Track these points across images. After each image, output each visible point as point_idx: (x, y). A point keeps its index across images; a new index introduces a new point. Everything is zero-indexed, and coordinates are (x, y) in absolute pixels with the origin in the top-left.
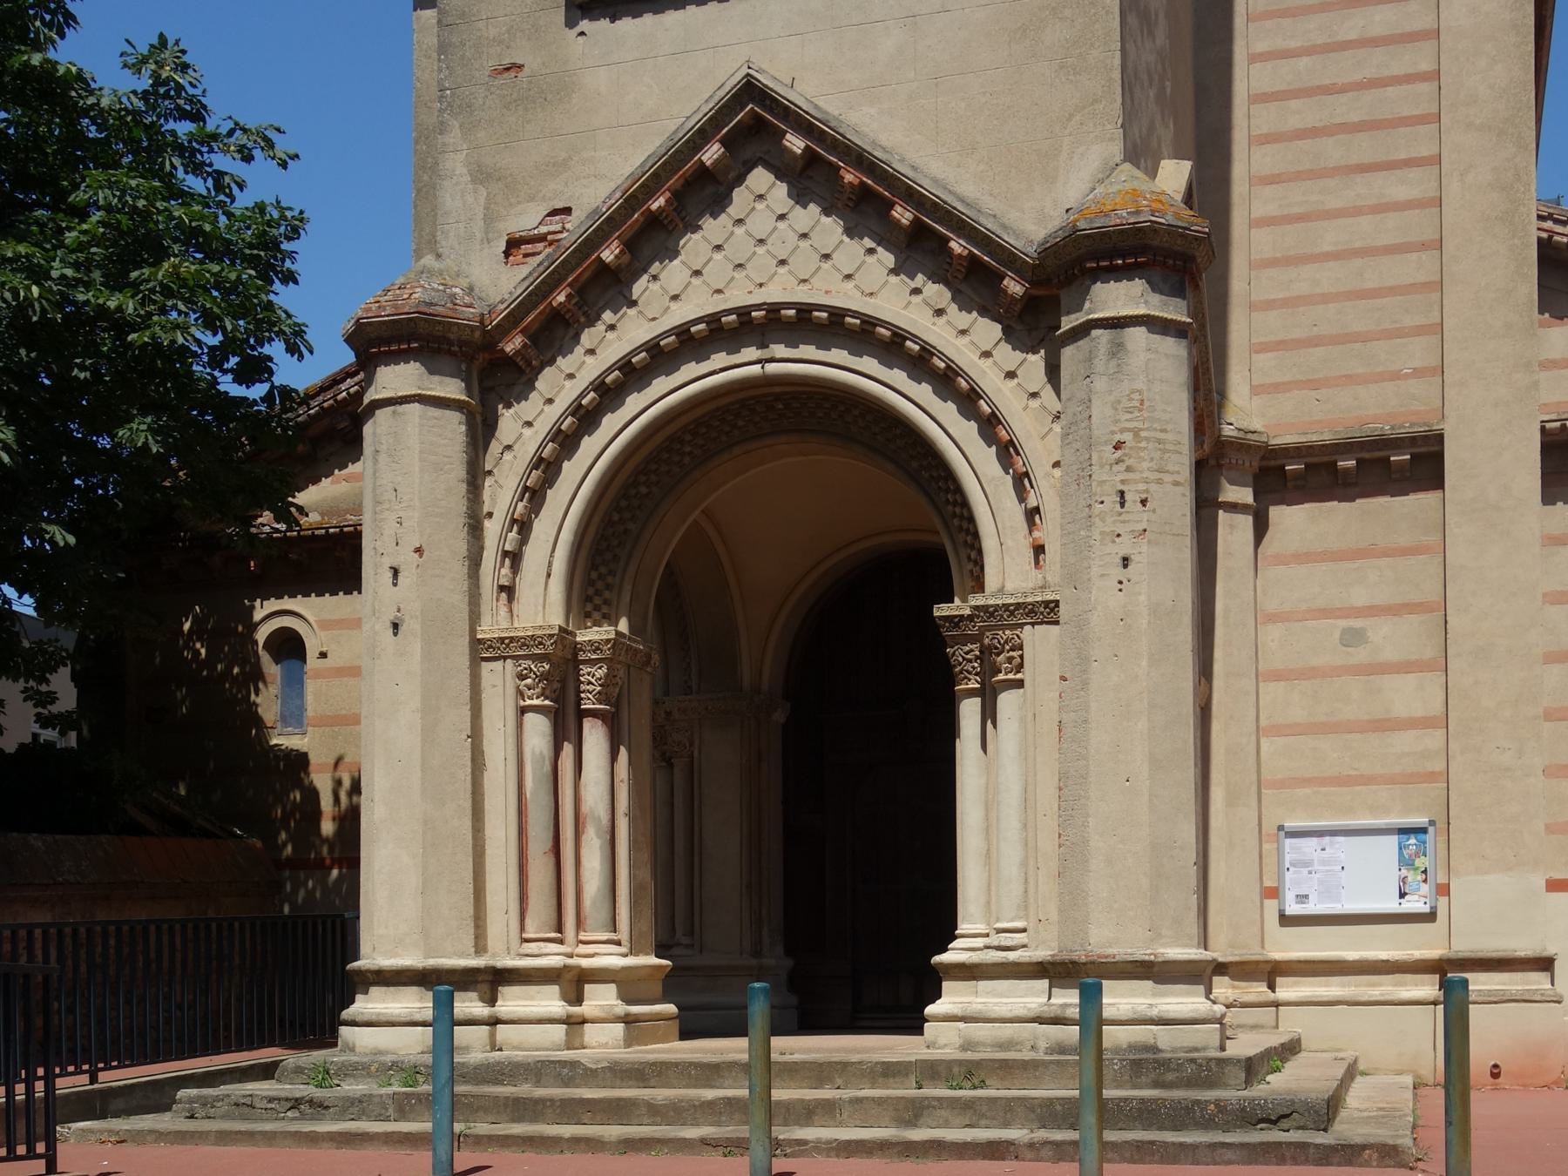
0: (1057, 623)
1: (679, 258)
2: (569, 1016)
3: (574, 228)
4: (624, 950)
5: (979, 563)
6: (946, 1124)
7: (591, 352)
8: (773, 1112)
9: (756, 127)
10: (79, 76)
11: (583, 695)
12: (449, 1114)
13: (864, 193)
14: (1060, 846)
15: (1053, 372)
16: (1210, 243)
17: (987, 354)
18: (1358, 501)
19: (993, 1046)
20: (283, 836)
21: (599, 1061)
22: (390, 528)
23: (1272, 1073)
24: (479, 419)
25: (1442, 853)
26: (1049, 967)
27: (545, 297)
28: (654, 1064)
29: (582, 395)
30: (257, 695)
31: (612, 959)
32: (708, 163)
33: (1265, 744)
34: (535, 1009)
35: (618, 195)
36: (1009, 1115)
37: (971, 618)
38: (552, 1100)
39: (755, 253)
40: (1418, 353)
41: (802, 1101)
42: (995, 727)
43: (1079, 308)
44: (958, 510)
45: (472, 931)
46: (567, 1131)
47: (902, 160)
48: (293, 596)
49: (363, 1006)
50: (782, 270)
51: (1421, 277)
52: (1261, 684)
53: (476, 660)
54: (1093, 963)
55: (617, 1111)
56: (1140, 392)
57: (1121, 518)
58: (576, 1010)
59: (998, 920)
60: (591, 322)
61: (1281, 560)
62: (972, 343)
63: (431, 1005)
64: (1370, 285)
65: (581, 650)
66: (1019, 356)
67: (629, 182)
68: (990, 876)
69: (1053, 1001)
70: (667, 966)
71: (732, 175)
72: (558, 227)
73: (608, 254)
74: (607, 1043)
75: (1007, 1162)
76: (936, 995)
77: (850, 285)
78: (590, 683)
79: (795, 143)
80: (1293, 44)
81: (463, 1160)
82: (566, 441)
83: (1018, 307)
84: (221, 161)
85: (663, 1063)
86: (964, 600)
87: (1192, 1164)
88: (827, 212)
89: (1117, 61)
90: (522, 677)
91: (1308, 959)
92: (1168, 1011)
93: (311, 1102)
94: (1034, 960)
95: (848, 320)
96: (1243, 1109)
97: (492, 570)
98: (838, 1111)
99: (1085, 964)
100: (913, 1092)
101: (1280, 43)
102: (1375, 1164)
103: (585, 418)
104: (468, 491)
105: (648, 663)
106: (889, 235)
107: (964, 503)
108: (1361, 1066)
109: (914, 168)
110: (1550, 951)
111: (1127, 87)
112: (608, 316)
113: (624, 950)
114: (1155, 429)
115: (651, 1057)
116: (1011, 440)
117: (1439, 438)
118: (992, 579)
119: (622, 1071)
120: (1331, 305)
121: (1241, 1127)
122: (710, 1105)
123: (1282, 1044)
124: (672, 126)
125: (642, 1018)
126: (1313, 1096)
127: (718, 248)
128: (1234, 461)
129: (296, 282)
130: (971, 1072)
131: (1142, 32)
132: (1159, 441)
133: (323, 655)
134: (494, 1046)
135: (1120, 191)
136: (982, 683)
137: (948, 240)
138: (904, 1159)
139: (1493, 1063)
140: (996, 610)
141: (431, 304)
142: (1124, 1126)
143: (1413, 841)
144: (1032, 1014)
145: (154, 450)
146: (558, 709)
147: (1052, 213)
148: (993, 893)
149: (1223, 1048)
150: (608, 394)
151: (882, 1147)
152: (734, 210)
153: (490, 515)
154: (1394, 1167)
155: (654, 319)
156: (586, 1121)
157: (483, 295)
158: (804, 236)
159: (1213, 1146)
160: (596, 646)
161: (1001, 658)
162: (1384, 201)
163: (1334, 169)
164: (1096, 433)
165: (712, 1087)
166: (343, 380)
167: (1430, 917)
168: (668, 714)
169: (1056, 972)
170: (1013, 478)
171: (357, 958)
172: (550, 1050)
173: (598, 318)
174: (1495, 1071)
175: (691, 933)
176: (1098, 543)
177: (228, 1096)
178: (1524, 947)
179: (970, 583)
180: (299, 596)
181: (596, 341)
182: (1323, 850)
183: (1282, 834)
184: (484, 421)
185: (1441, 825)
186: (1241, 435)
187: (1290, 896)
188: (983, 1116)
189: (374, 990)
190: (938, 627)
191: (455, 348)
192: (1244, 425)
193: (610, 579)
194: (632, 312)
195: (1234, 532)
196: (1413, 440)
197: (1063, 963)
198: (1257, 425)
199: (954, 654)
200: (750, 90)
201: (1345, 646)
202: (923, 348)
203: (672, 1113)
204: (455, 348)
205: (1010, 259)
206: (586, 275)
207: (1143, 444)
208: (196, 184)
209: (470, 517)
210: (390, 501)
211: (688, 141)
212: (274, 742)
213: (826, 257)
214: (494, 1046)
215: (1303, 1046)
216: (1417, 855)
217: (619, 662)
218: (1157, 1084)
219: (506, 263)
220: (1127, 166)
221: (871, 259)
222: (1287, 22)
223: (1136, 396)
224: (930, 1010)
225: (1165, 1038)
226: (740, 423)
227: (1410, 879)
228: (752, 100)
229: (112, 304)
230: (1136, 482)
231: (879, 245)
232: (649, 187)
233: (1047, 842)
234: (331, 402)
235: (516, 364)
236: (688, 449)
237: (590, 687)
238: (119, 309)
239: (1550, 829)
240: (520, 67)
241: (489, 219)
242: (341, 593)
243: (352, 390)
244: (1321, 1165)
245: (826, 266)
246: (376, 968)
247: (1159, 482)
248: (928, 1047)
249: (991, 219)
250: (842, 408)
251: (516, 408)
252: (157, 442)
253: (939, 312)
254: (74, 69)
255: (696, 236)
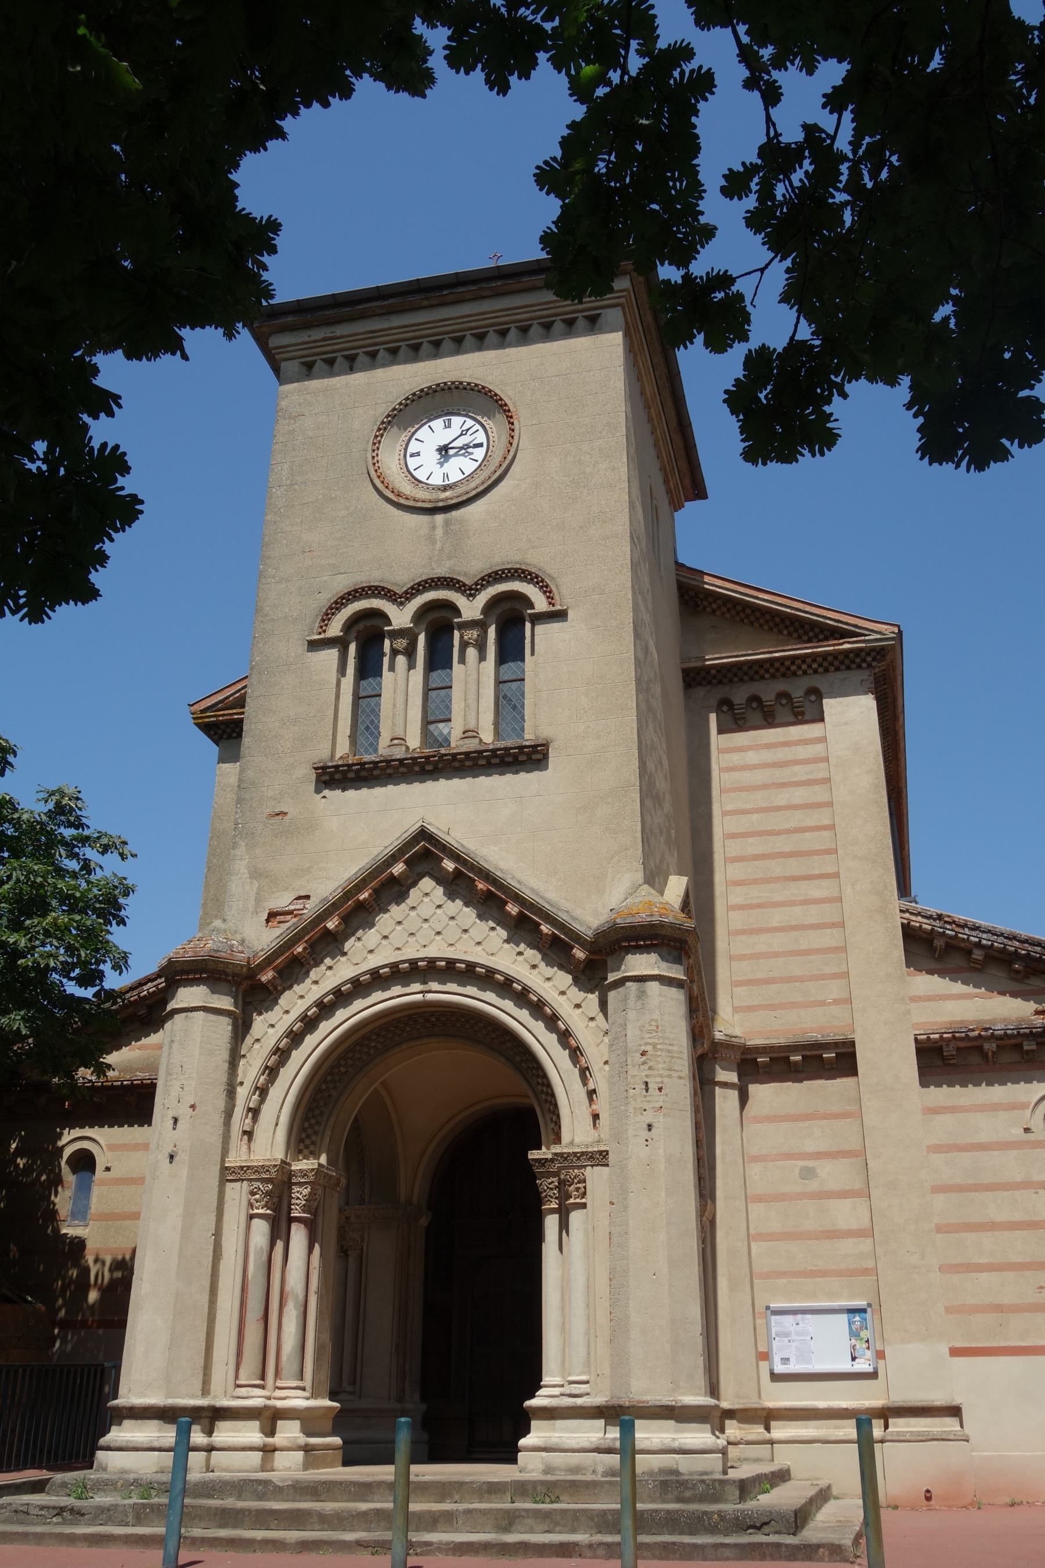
0: (607, 1165)
1: (375, 928)
2: (265, 1446)
3: (311, 908)
4: (307, 1394)
5: (558, 1123)
6: (532, 1531)
7: (316, 982)
8: (409, 1521)
9: (426, 855)
10: (10, 801)
11: (292, 1207)
12: (179, 1517)
13: (489, 896)
14: (611, 1321)
15: (603, 1005)
16: (697, 933)
17: (563, 993)
18: (805, 1082)
19: (565, 1471)
20: (60, 1302)
21: (285, 1480)
22: (175, 1091)
23: (763, 1493)
24: (240, 1022)
25: (878, 1327)
26: (604, 1410)
27: (289, 949)
28: (325, 1483)
29: (308, 1009)
30: (56, 1196)
31: (298, 1401)
32: (396, 874)
33: (754, 1246)
34: (241, 1440)
35: (340, 890)
36: (575, 1523)
37: (552, 1160)
38: (250, 1511)
39: (421, 927)
40: (834, 990)
41: (430, 1511)
42: (568, 1235)
43: (618, 969)
44: (545, 1089)
45: (201, 1378)
46: (260, 1534)
47: (513, 878)
48: (92, 1126)
49: (117, 1434)
50: (438, 938)
51: (834, 943)
52: (749, 1204)
53: (223, 1181)
54: (633, 1407)
55: (296, 1519)
56: (656, 1021)
57: (646, 1099)
58: (270, 1440)
59: (570, 1375)
60: (317, 964)
61: (758, 1120)
62: (554, 986)
63: (175, 1435)
64: (804, 947)
65: (294, 1175)
66: (582, 995)
67: (347, 883)
68: (564, 1342)
69: (607, 1435)
70: (337, 1407)
71: (409, 881)
72: (301, 907)
73: (331, 925)
74: (290, 1467)
75: (574, 1559)
76: (526, 1431)
77: (479, 948)
78: (298, 1198)
79: (449, 865)
80: (748, 806)
81: (184, 1557)
82: (295, 1038)
83: (582, 966)
84: (90, 853)
85: (331, 1482)
86: (548, 1148)
87: (702, 1560)
88: (467, 904)
89: (639, 828)
90: (253, 1193)
91: (792, 1407)
92: (685, 1444)
93: (72, 1510)
94: (594, 1404)
95: (478, 969)
96: (737, 1518)
97: (239, 1120)
98: (455, 1520)
99: (628, 1408)
100: (508, 1506)
101: (740, 806)
102: (827, 1559)
103: (309, 1023)
104: (229, 1068)
105: (338, 1184)
106: (503, 920)
107: (549, 1085)
108: (835, 1491)
109: (519, 882)
110: (957, 1401)
111: (646, 840)
112: (328, 961)
113: (307, 1394)
114: (666, 1044)
115: (323, 1478)
116: (578, 1047)
117: (852, 1044)
118: (566, 1136)
119: (300, 1488)
120: (780, 959)
121: (736, 1532)
122: (365, 1514)
123: (772, 1472)
124: (375, 852)
125: (318, 1448)
126: (785, 1508)
127: (399, 923)
128: (724, 1055)
129: (125, 924)
130: (549, 1489)
131: (655, 807)
132: (669, 1051)
133: (108, 1169)
134: (209, 1469)
135: (641, 902)
136: (560, 1204)
137: (540, 924)
138: (500, 1557)
139: (925, 1489)
140: (568, 1156)
141: (218, 951)
142: (655, 1532)
143: (857, 1318)
144: (593, 1446)
145: (24, 1033)
146: (275, 1217)
147: (602, 911)
148: (567, 1355)
149: (725, 1473)
150: (325, 1009)
151: (485, 1548)
152: (410, 901)
153: (242, 1083)
154: (840, 1561)
155: (357, 964)
156: (273, 1527)
157: (251, 945)
158: (453, 918)
159: (717, 1546)
160: (304, 1173)
161: (572, 1188)
162: (808, 897)
163: (777, 878)
164: (630, 1045)
165: (366, 1501)
166: (146, 984)
167: (873, 1375)
168: (347, 1218)
169: (609, 1413)
170: (580, 1070)
171: (116, 1397)
172: (249, 1472)
173: (322, 961)
174: (928, 1495)
175: (354, 1383)
176: (632, 1115)
177: (11, 1504)
178: (939, 1398)
179: (552, 1137)
180: (96, 1127)
181: (320, 976)
182: (797, 1324)
183: (769, 1312)
184: (244, 1023)
185: (875, 1307)
186: (728, 1038)
187: (777, 1359)
188: (557, 1524)
189: (127, 1423)
190: (531, 1166)
191: (230, 978)
192: (730, 1032)
193: (316, 1128)
194: (343, 959)
195: (726, 1102)
196: (836, 1045)
197: (613, 1407)
198: (737, 1031)
199: (541, 1184)
200: (423, 834)
201: (803, 1179)
202: (523, 988)
203: (336, 1521)
204: (230, 978)
205: (577, 938)
206: (316, 936)
207: (659, 1053)
208: (73, 865)
209: (229, 1085)
210: (177, 1074)
211: (384, 861)
212: (64, 1231)
213: (466, 931)
214: (209, 1469)
215: (792, 1476)
216: (861, 1328)
217: (319, 1185)
218: (680, 1500)
219: (267, 927)
220: (646, 886)
221: (493, 934)
222: (744, 794)
223: (654, 1023)
224: (523, 1442)
225: (685, 1464)
226: (408, 1029)
227: (858, 1347)
228: (424, 840)
229: (11, 940)
230: (655, 1076)
231: (498, 925)
232: (360, 886)
233: (602, 1318)
234: (136, 997)
235: (267, 989)
236: (373, 1044)
237: (298, 1202)
238: (15, 943)
239: (948, 1310)
240: (286, 814)
241: (258, 900)
242: (126, 1126)
243: (151, 990)
244: (790, 1560)
245: (465, 936)
246: (130, 1405)
247: (670, 1076)
248: (521, 1472)
249: (566, 914)
250: (472, 1022)
251: (265, 1015)
252: (26, 1027)
253: (534, 967)
254: (8, 798)
255: (386, 916)
